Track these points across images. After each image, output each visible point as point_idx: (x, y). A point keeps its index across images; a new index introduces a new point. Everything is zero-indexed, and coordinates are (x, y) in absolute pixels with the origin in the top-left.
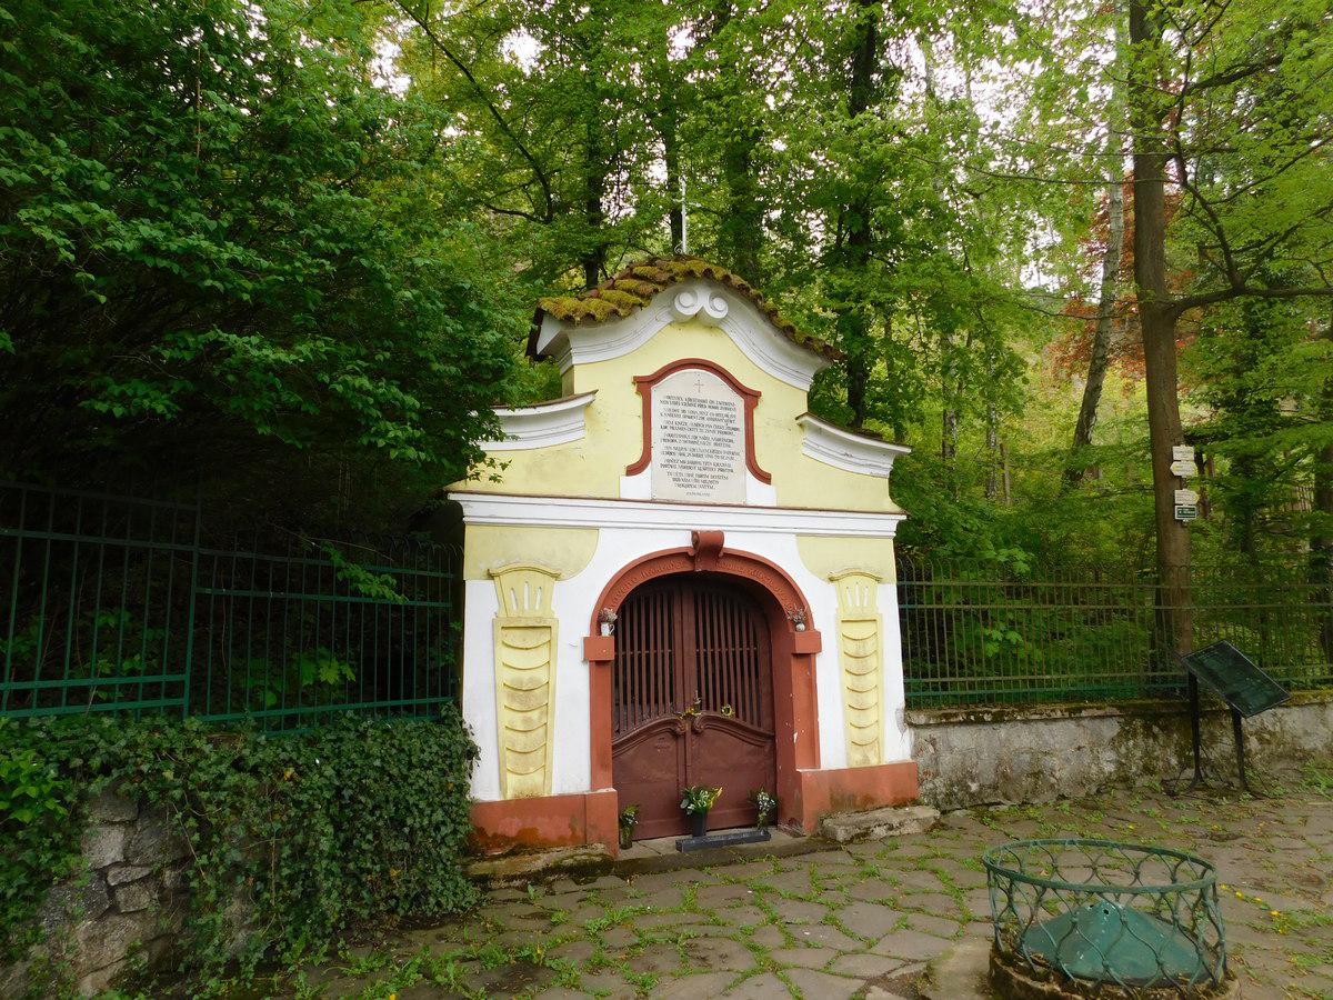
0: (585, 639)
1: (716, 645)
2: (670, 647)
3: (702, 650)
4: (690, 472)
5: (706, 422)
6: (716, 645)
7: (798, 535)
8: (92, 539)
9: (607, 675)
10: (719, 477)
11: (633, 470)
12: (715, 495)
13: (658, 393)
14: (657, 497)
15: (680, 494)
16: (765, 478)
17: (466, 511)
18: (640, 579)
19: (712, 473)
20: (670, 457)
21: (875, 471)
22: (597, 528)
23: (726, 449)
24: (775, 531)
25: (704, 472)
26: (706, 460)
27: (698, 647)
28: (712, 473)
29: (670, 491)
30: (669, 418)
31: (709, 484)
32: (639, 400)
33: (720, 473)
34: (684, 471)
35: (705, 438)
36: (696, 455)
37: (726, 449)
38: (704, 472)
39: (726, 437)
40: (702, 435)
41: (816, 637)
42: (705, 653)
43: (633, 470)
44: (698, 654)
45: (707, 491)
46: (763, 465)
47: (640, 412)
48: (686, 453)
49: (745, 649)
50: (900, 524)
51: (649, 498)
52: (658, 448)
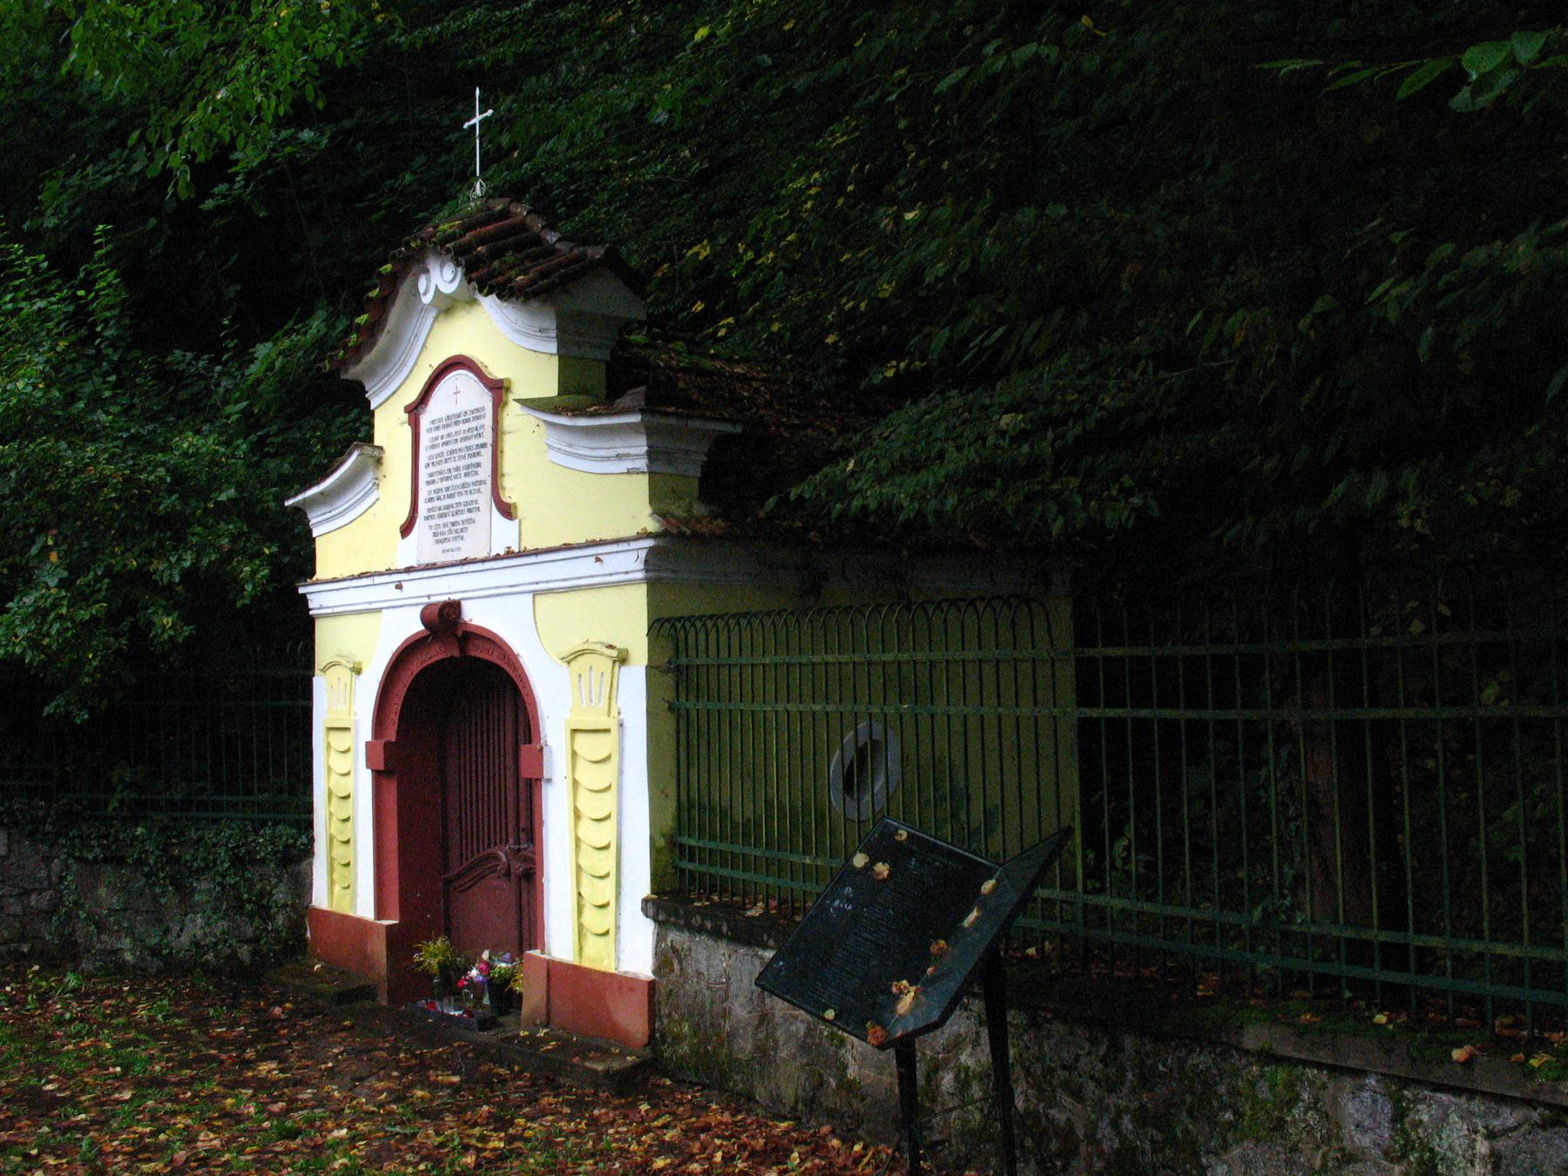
0: (367, 743)
7: (535, 593)
11: (406, 530)
13: (425, 420)
16: (507, 511)
22: (379, 610)
24: (511, 592)
43: (406, 530)
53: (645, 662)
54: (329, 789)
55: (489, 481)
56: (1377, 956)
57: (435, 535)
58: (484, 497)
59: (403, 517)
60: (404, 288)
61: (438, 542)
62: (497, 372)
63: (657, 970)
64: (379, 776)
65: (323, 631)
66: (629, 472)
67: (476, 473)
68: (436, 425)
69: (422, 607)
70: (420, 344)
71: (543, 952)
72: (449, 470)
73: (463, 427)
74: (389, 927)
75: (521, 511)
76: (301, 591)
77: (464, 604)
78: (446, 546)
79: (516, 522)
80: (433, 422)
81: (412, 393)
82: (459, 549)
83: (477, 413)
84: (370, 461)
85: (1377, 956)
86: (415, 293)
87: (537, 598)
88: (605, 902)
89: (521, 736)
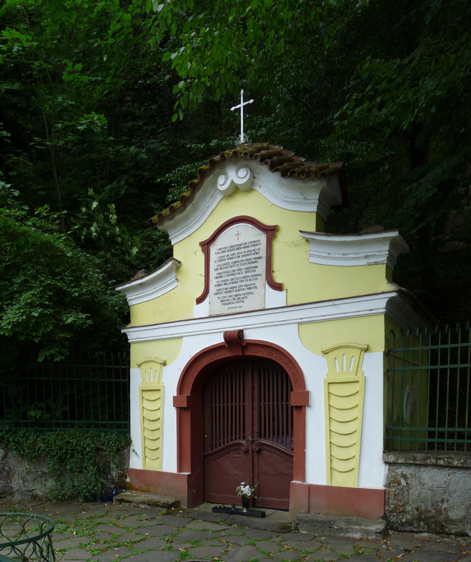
0: (174, 397)
1: (222, 407)
2: (260, 405)
3: (262, 403)
4: (230, 294)
5: (241, 259)
6: (222, 407)
7: (299, 324)
8: (118, 380)
9: (187, 416)
10: (248, 294)
11: (200, 300)
12: (246, 306)
13: (214, 249)
14: (212, 314)
15: (225, 310)
16: (278, 287)
17: (129, 337)
18: (205, 362)
19: (244, 292)
20: (219, 288)
21: (373, 260)
22: (181, 337)
23: (253, 274)
24: (283, 323)
25: (238, 293)
26: (239, 284)
27: (244, 406)
28: (244, 292)
29: (221, 309)
30: (220, 263)
31: (241, 300)
32: (202, 256)
33: (249, 291)
34: (227, 295)
35: (240, 270)
36: (234, 283)
37: (253, 274)
38: (238, 293)
39: (252, 265)
40: (238, 268)
41: (306, 396)
42: (220, 403)
43: (200, 300)
44: (244, 401)
45: (241, 304)
46: (278, 279)
47: (203, 273)
48: (228, 282)
49: (221, 405)
50: (391, 302)
51: (207, 316)
52: (212, 289)
53: (383, 349)
54: (144, 417)
55: (264, 275)
56: (61, 425)
57: (222, 301)
58: (261, 281)
59: (200, 293)
60: (207, 181)
61: (224, 304)
62: (268, 222)
63: (388, 485)
64: (181, 411)
65: (133, 349)
66: (369, 264)
67: (255, 271)
68: (222, 250)
69: (388, 299)
70: (210, 210)
71: (304, 479)
72: (234, 271)
73: (243, 250)
74: (188, 475)
75: (286, 286)
76: (123, 331)
77: (245, 331)
78: (230, 306)
79: (284, 292)
80: (220, 249)
81: (206, 235)
82: (241, 307)
83: (255, 243)
84: (175, 267)
85: (61, 425)
86: (215, 183)
87: (300, 326)
88: (353, 456)
89: (289, 388)
